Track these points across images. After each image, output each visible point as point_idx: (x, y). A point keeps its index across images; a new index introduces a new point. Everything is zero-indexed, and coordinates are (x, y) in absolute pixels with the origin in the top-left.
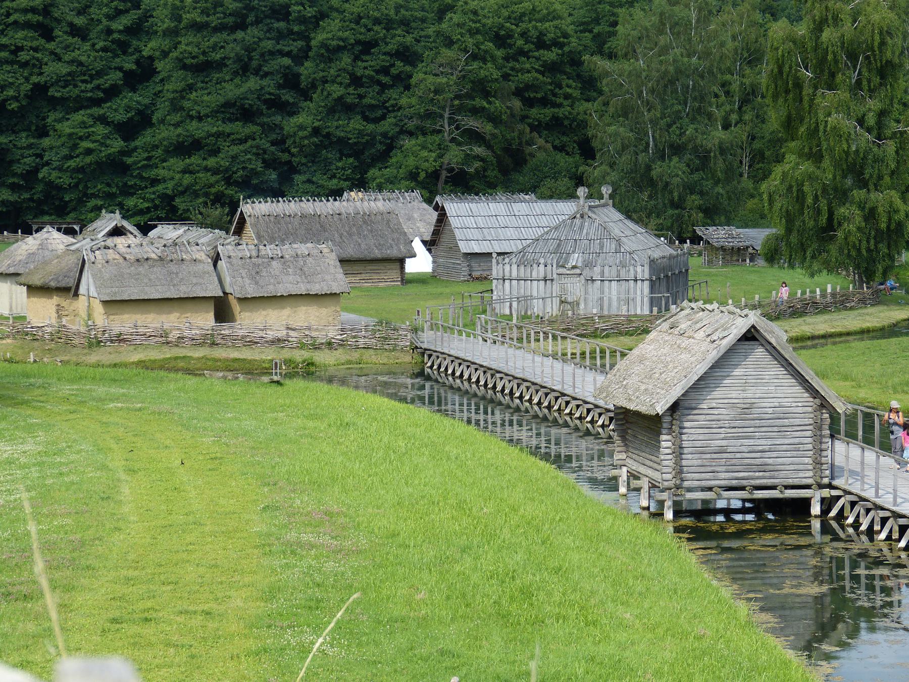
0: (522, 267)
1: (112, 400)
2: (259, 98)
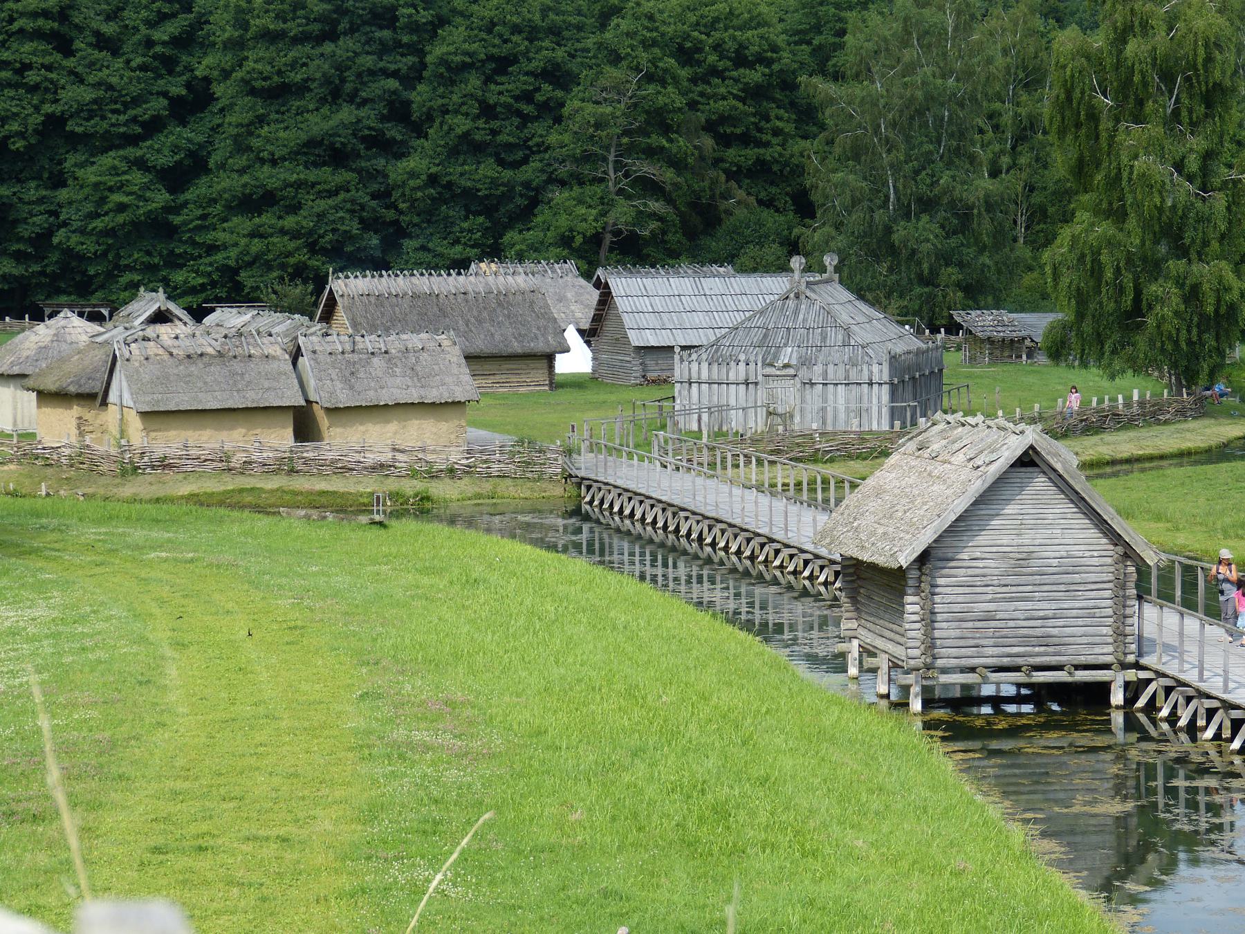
0: (715, 366)
2: (354, 135)
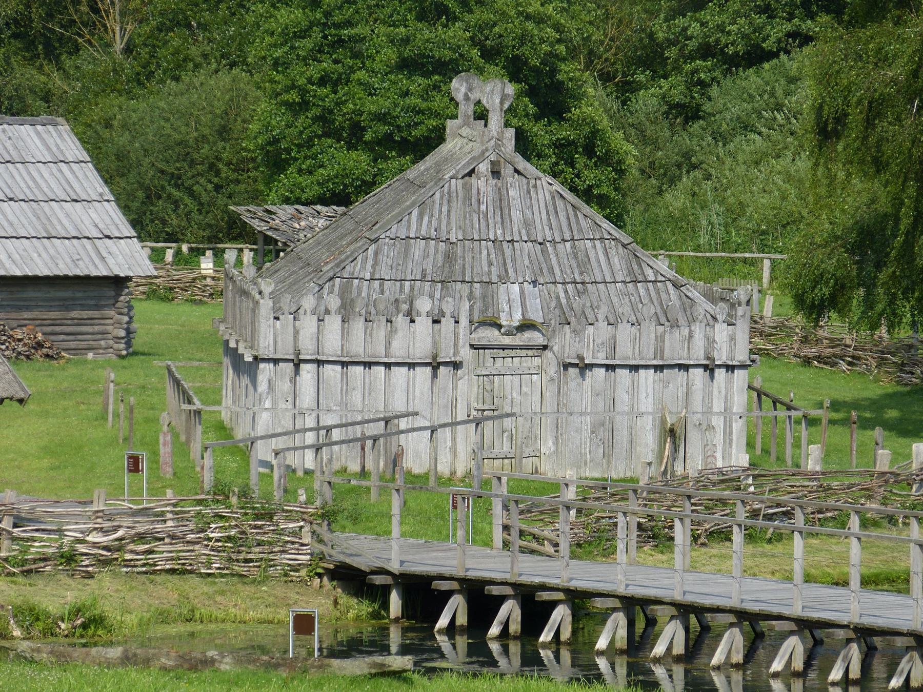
0: (358, 325)
1: (227, 574)
